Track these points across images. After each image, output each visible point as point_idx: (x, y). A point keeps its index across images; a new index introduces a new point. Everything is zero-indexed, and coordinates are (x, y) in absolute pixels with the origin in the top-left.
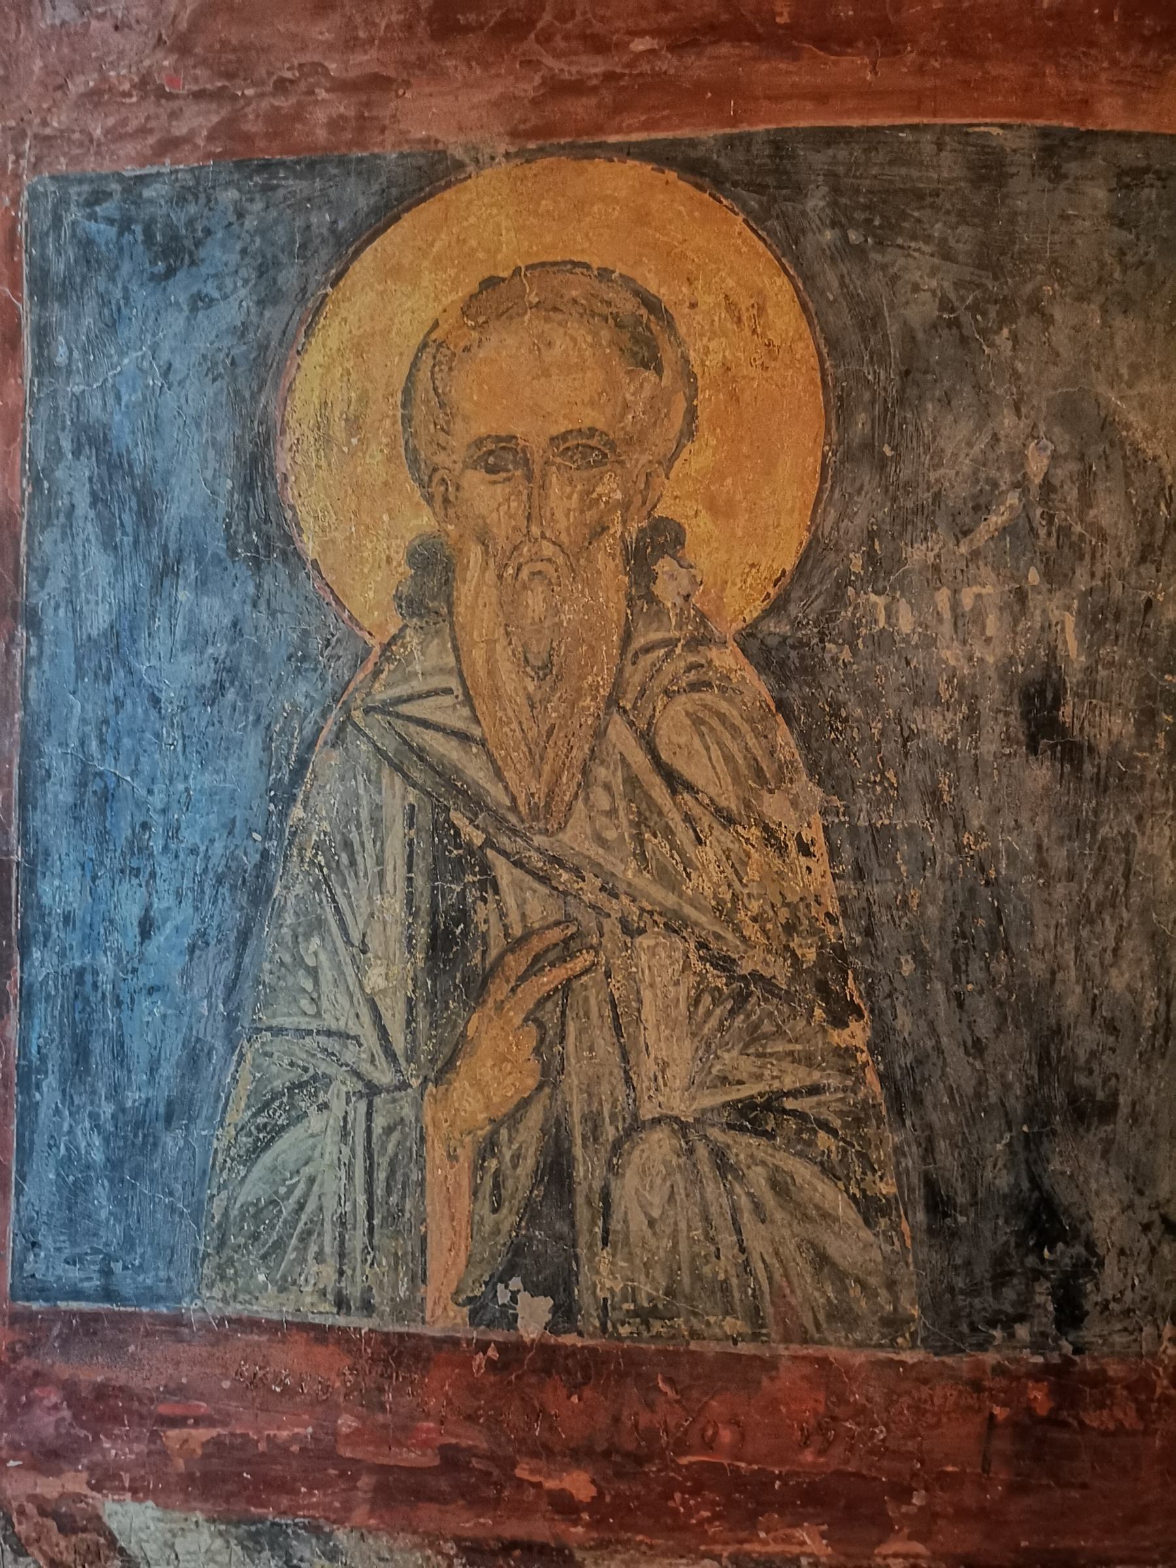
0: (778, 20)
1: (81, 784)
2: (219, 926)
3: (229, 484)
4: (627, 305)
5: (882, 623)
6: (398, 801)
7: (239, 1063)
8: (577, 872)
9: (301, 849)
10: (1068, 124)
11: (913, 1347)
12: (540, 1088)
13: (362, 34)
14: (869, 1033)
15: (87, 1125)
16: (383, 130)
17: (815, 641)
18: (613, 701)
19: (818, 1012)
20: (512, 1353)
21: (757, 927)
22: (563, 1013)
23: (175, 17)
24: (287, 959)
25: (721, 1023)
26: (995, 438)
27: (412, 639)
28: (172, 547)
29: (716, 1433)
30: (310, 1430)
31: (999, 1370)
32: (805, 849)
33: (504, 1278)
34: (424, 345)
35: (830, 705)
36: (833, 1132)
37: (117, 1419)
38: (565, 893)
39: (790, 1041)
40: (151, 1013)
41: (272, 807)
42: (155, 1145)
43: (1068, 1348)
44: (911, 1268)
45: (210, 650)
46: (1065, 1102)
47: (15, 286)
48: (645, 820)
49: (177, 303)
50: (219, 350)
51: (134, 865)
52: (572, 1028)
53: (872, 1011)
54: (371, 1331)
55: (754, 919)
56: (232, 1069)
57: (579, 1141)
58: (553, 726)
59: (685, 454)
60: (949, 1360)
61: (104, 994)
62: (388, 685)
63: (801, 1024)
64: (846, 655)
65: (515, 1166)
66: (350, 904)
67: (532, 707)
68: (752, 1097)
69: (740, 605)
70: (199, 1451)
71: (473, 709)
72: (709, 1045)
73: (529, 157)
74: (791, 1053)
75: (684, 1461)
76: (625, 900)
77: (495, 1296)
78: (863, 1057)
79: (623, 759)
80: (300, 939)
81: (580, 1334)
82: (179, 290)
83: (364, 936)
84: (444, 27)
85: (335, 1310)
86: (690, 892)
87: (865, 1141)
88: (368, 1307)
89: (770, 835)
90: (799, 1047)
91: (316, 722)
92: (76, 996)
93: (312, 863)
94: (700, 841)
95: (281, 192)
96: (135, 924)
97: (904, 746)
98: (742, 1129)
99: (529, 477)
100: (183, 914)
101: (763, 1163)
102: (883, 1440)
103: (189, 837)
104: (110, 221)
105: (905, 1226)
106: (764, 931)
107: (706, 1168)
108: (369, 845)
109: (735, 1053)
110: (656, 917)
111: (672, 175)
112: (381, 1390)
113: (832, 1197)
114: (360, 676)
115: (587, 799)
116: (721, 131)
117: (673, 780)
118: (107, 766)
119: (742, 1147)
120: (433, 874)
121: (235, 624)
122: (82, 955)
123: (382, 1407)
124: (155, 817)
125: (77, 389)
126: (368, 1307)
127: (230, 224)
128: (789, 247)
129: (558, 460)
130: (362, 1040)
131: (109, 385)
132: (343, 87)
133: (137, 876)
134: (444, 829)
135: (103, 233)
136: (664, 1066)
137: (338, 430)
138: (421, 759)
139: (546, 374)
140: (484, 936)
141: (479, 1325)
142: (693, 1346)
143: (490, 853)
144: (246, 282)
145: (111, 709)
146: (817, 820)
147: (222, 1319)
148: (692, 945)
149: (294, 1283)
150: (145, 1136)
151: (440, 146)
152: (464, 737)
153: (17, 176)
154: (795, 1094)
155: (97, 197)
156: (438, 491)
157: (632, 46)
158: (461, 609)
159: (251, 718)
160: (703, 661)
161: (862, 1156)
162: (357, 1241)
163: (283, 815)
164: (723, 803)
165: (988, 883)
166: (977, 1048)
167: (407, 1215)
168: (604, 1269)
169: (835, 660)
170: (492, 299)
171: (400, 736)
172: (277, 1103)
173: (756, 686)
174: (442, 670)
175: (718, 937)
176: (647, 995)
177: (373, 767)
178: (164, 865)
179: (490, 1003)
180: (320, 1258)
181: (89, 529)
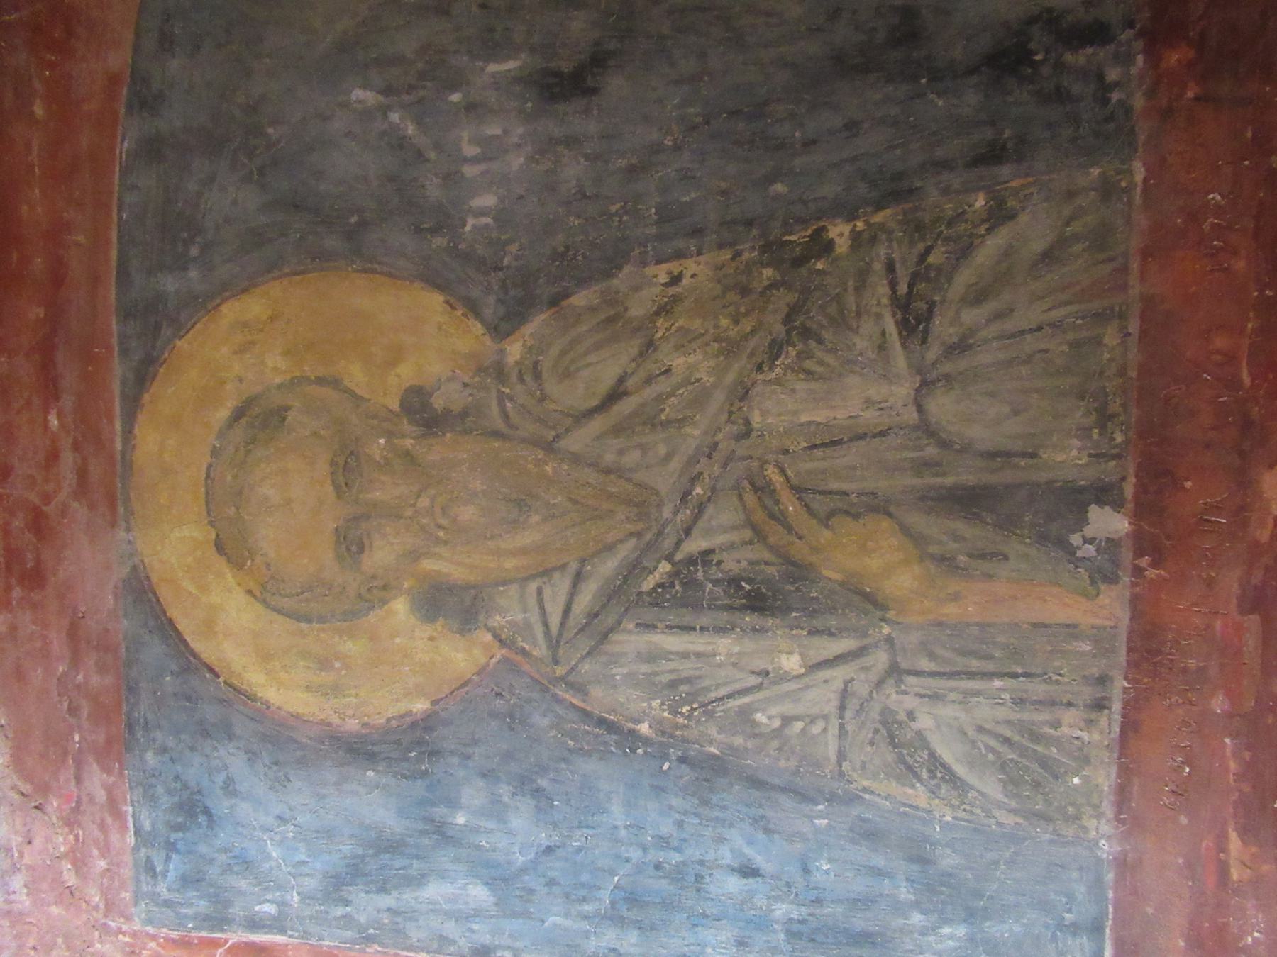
0: (42, 316)
1: (619, 921)
2: (747, 805)
3: (370, 773)
4: (239, 433)
5: (488, 220)
6: (633, 638)
7: (872, 793)
8: (694, 480)
9: (677, 726)
10: (125, 91)
11: (1130, 172)
12: (890, 515)
13: (39, 644)
14: (839, 221)
15: (931, 938)
16: (107, 630)
17: (500, 274)
18: (549, 448)
19: (820, 266)
20: (1145, 544)
21: (744, 320)
22: (821, 493)
23: (22, 794)
24: (775, 744)
25: (829, 351)
26: (348, 134)
27: (497, 620)
28: (420, 826)
29: (1218, 352)
30: (1227, 740)
31: (1151, 94)
32: (675, 280)
33: (1071, 551)
34: (265, 603)
35: (554, 261)
36: (928, 251)
37: (1221, 929)
38: (713, 490)
39: (845, 290)
40: (827, 872)
41: (639, 751)
42: (950, 875)
43: (1129, 33)
44: (1055, 176)
45: (506, 799)
46: (901, 48)
47: (215, 944)
48: (650, 419)
49: (232, 807)
50: (265, 774)
51: (693, 879)
52: (835, 485)
53: (819, 219)
54: (1126, 678)
55: (736, 322)
56: (878, 800)
57: (939, 480)
58: (570, 499)
59: (352, 386)
60: (1142, 138)
61: (811, 915)
62: (535, 644)
63: (829, 280)
64: (513, 248)
65: (964, 539)
66: (725, 684)
67: (553, 517)
68: (896, 322)
69: (471, 337)
70: (1254, 849)
71: (554, 569)
72: (849, 362)
73: (130, 513)
74: (857, 289)
75: (1246, 379)
76: (720, 436)
77: (1089, 559)
78: (860, 225)
79: (598, 438)
80: (757, 731)
81: (1123, 479)
82: (221, 805)
83: (753, 673)
84: (35, 578)
85: (1106, 711)
86: (711, 380)
87: (938, 220)
88: (1102, 680)
89: (664, 310)
90: (851, 283)
91: (567, 708)
92: (813, 940)
93: (689, 718)
94: (667, 371)
95: (150, 717)
96: (745, 881)
97: (589, 198)
98: (926, 332)
99: (367, 517)
100: (736, 837)
101: (958, 312)
102: (1223, 197)
103: (667, 828)
104: (168, 859)
105: (1015, 184)
106: (747, 314)
107: (962, 364)
108: (671, 666)
109: (857, 340)
110: (734, 409)
111: (146, 397)
112: (1185, 671)
113: (991, 247)
114: (526, 667)
115: (631, 470)
116: (116, 360)
117: (616, 395)
118: (605, 895)
119: (944, 328)
120: (697, 607)
121: (484, 775)
122: (775, 931)
123: (1201, 670)
124: (650, 857)
125: (296, 898)
126: (1102, 680)
127: (171, 759)
128: (201, 304)
129: (354, 491)
130: (848, 677)
131: (293, 871)
132: (76, 662)
133: (702, 877)
134: (657, 598)
135: (176, 867)
136: (869, 402)
137: (327, 677)
138: (596, 615)
139: (288, 502)
140: (751, 563)
141: (1117, 576)
142: (1134, 374)
143: (679, 556)
144: (215, 748)
145: (556, 890)
146: (650, 270)
147: (1119, 821)
148: (760, 377)
149: (1081, 749)
150: (942, 885)
151: (120, 585)
152: (578, 578)
153: (134, 935)
154: (893, 285)
155: (150, 868)
156: (377, 592)
157: (54, 429)
158: (472, 578)
159: (563, 766)
160: (516, 370)
161: (950, 224)
162: (1038, 689)
163: (646, 741)
164: (635, 351)
165: (708, 123)
166: (852, 127)
167: (1012, 640)
168: (1060, 457)
169: (517, 258)
170: (231, 547)
171: (577, 634)
172: (908, 759)
173: (537, 324)
174: (522, 598)
175: (752, 354)
176: (804, 418)
177: (604, 659)
178: (693, 852)
179: (813, 559)
180: (1056, 724)
181: (408, 896)
